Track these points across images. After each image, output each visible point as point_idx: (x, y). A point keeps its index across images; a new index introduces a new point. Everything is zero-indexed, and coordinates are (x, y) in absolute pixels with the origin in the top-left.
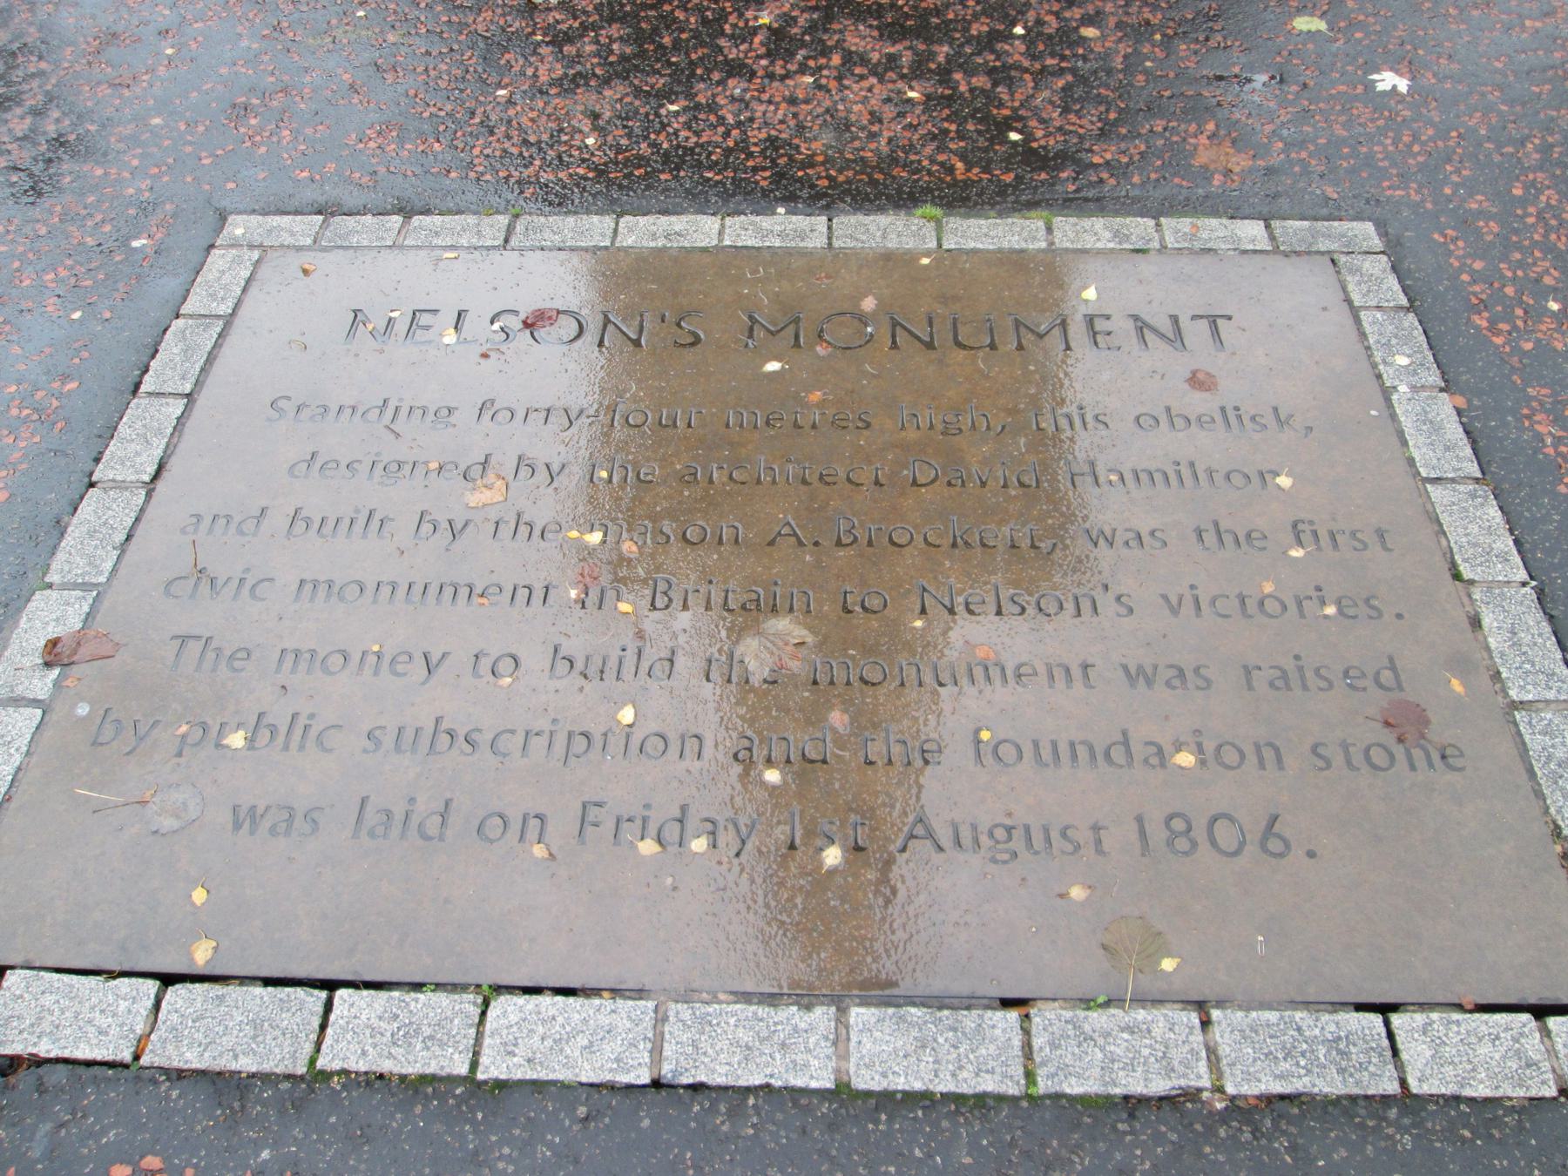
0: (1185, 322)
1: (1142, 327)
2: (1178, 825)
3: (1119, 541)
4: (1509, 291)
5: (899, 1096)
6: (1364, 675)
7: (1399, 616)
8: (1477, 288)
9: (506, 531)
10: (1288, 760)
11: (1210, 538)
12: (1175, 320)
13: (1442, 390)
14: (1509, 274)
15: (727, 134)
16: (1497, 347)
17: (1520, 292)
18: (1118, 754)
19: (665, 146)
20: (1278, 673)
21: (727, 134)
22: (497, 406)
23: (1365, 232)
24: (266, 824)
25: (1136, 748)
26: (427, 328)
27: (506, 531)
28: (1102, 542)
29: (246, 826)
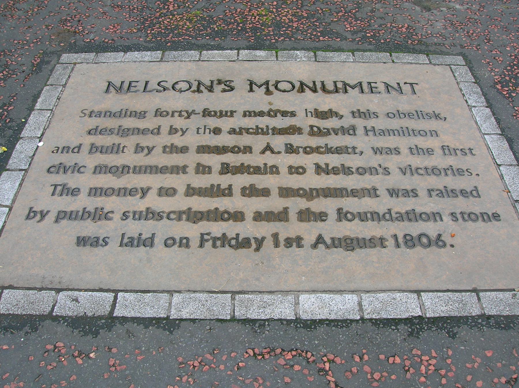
0: (402, 85)
1: (387, 86)
2: (408, 238)
3: (384, 152)
4: (507, 78)
5: (318, 321)
6: (467, 193)
7: (478, 175)
8: (497, 77)
9: (201, 131)
10: (444, 218)
11: (415, 151)
12: (398, 84)
13: (487, 107)
14: (507, 73)
15: (238, 25)
16: (505, 95)
17: (510, 79)
18: (387, 216)
19: (216, 29)
20: (405, 191)
21: (238, 25)
22: (162, 110)
23: (460, 60)
24: (90, 242)
25: (394, 215)
26: (135, 86)
27: (201, 131)
28: (378, 152)
29: (82, 243)
